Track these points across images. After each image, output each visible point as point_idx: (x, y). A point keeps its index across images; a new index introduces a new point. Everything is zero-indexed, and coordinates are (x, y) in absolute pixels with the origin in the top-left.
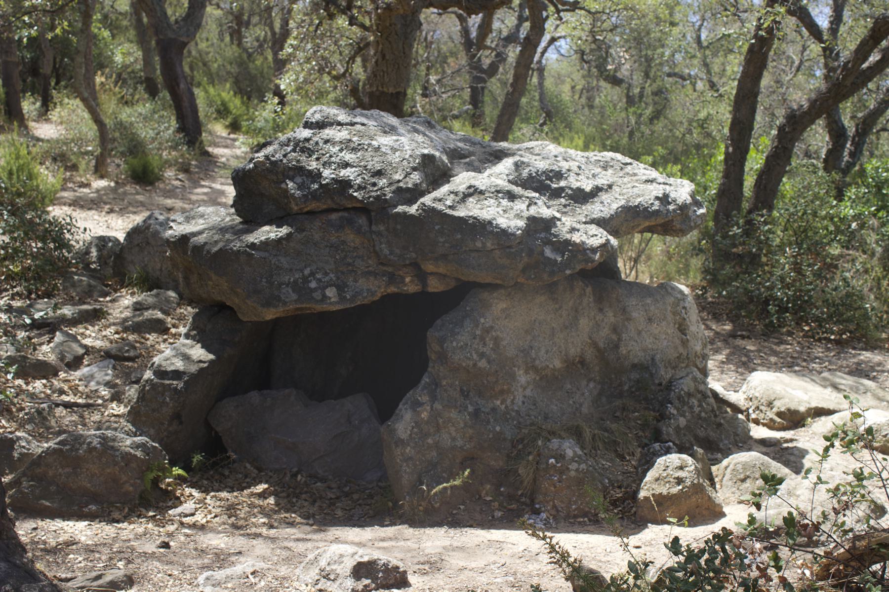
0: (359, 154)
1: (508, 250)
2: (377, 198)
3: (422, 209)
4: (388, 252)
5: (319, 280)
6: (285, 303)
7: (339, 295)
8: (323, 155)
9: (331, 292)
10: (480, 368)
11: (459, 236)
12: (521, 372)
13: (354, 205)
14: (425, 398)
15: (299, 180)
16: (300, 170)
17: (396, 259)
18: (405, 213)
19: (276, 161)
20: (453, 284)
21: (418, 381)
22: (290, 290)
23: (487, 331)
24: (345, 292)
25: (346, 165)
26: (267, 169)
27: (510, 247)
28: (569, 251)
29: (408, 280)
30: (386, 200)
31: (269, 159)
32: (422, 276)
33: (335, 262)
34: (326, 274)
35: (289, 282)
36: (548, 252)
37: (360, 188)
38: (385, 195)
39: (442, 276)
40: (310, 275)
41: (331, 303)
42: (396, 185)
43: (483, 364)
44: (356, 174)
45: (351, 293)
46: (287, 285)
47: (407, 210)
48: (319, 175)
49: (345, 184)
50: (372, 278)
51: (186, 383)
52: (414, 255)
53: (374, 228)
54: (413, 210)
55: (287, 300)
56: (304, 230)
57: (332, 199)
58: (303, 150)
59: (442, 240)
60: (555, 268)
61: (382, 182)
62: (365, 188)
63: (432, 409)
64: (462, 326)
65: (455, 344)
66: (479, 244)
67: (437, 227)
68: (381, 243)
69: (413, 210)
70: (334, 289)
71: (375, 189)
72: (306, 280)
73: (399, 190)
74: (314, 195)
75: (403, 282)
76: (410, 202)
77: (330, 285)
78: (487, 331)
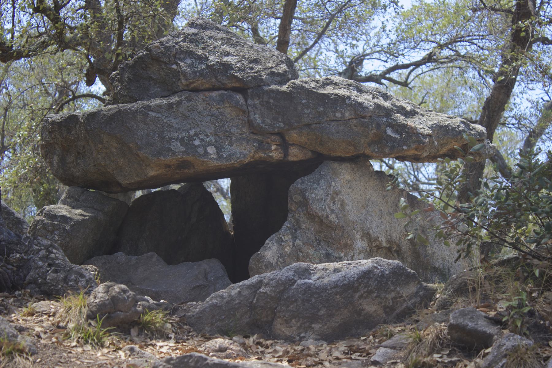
0: (237, 48)
1: (362, 120)
2: (254, 78)
3: (293, 87)
4: (260, 122)
5: (202, 140)
6: (174, 153)
7: (218, 153)
8: (208, 46)
9: (211, 150)
10: (331, 222)
11: (322, 109)
12: (359, 237)
13: (233, 85)
14: (288, 237)
15: (189, 61)
16: (189, 53)
17: (267, 127)
18: (278, 90)
19: (170, 47)
20: (309, 155)
21: (280, 227)
22: (179, 144)
23: (337, 193)
24: (222, 152)
25: (228, 54)
26: (161, 52)
27: (364, 117)
28: (406, 132)
29: (273, 147)
30: (262, 79)
31: (163, 45)
32: (285, 145)
33: (215, 128)
34: (207, 136)
35: (178, 138)
36: (389, 131)
37: (239, 69)
38: (261, 76)
39: (301, 147)
40: (194, 135)
41: (211, 158)
42: (270, 70)
43: (333, 218)
44: (237, 60)
45: (227, 154)
46: (176, 140)
47: (279, 88)
48: (207, 59)
49: (227, 66)
50: (245, 143)
51: (72, 226)
52: (282, 125)
53: (250, 102)
54: (284, 88)
55: (176, 150)
56: (191, 101)
57: (216, 77)
58: (191, 42)
59: (307, 112)
60: (395, 144)
61: (258, 67)
62: (244, 70)
63: (294, 245)
64: (319, 184)
65: (313, 196)
66: (338, 115)
67: (304, 102)
68: (255, 114)
69: (284, 88)
70: (214, 148)
71: (253, 71)
72: (191, 138)
73: (273, 74)
74: (202, 74)
75: (269, 149)
76: (281, 83)
77: (210, 144)
78: (337, 193)
